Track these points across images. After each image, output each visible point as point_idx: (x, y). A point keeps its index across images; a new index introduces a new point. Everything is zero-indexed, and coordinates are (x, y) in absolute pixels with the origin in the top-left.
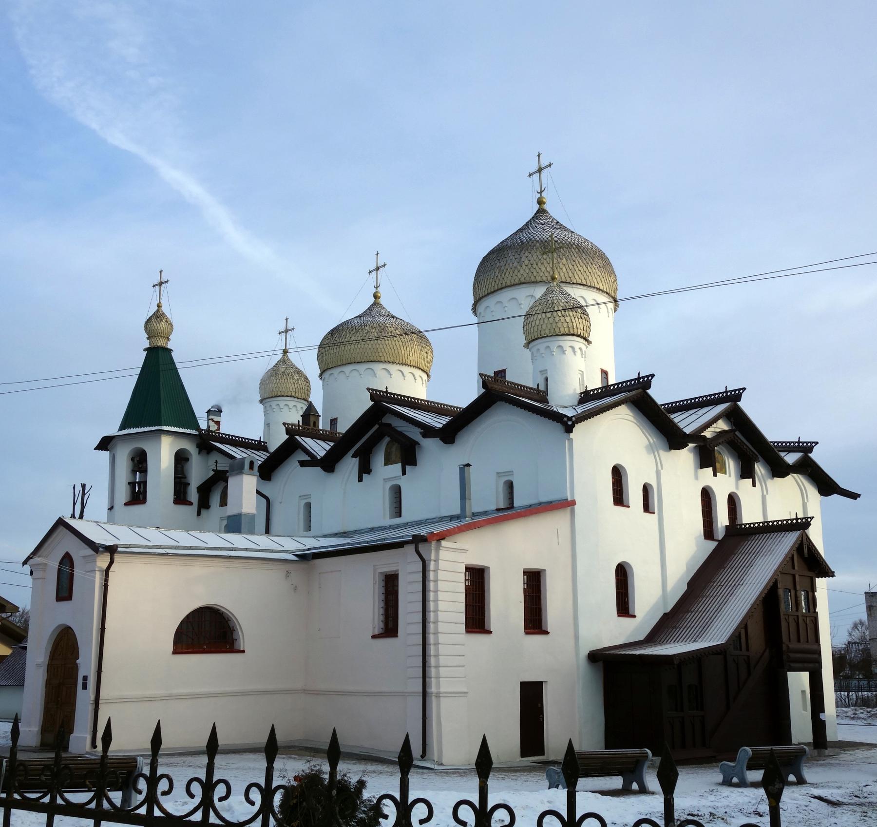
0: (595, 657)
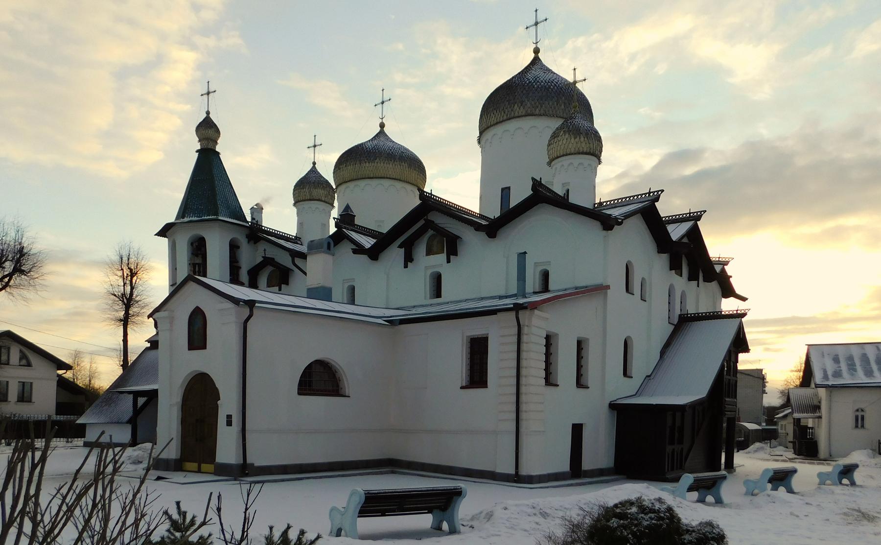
0: (613, 406)
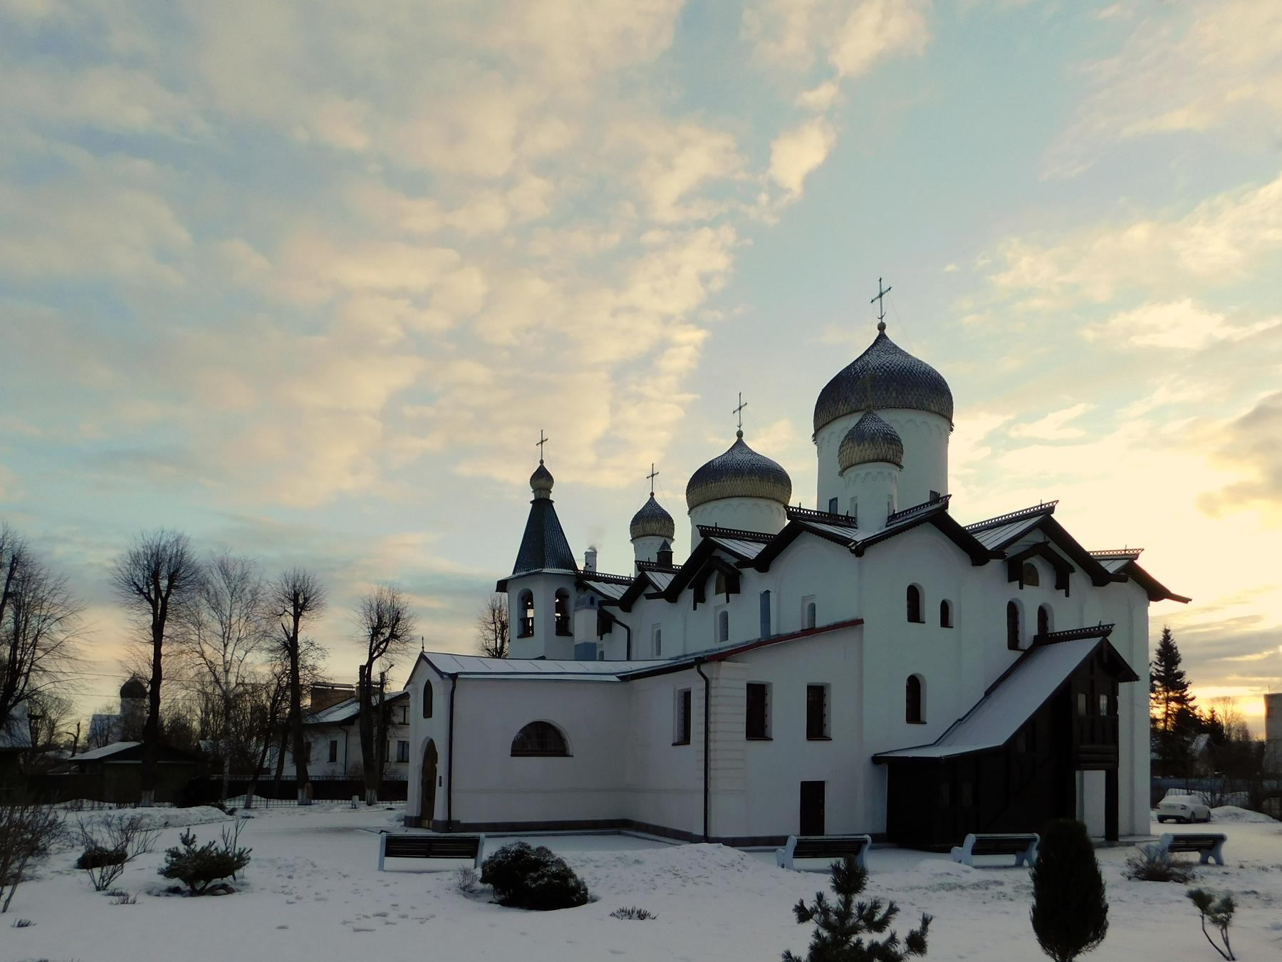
0: (877, 760)
